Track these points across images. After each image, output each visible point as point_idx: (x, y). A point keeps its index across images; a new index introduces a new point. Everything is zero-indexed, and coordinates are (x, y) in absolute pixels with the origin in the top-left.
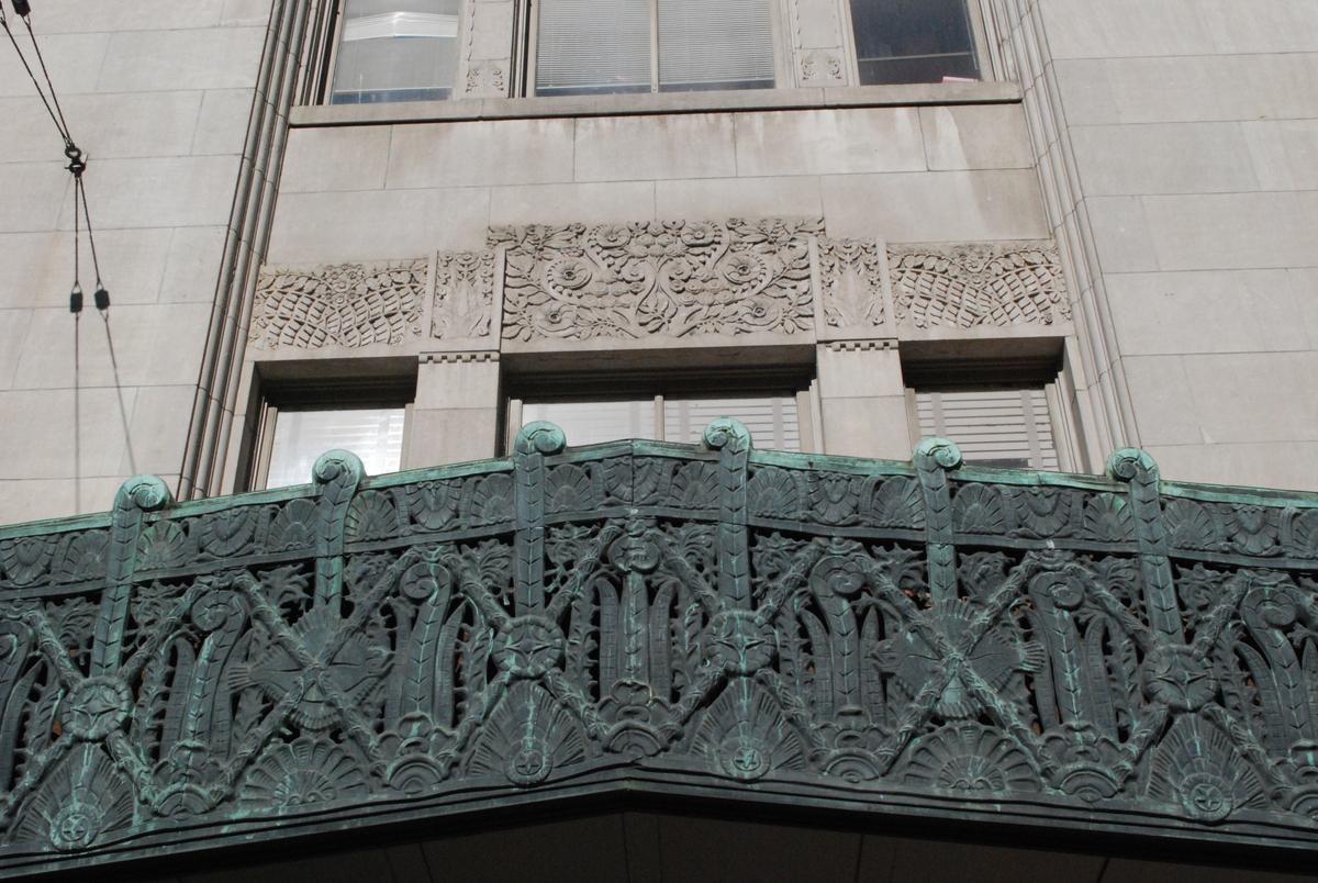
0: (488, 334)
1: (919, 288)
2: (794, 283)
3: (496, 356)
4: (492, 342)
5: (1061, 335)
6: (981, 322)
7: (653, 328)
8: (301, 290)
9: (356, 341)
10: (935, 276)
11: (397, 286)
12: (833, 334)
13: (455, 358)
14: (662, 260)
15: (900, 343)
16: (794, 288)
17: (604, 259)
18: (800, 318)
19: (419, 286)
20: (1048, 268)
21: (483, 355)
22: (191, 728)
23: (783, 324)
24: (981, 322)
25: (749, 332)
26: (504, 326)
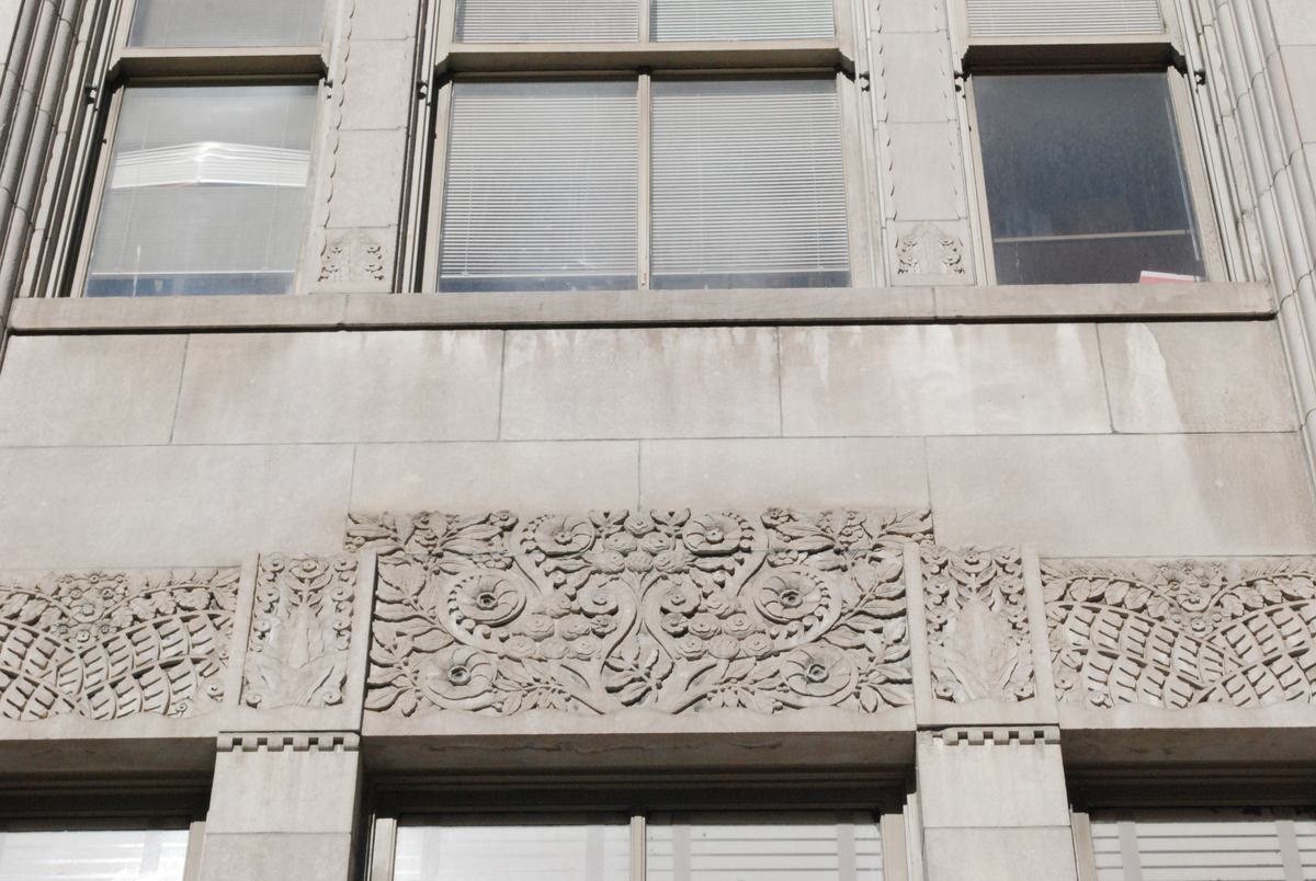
2: (879, 623)
6: (1205, 699)
10: (1124, 616)
12: (945, 714)
23: (857, 696)
24: (1205, 699)
26: (368, 687)
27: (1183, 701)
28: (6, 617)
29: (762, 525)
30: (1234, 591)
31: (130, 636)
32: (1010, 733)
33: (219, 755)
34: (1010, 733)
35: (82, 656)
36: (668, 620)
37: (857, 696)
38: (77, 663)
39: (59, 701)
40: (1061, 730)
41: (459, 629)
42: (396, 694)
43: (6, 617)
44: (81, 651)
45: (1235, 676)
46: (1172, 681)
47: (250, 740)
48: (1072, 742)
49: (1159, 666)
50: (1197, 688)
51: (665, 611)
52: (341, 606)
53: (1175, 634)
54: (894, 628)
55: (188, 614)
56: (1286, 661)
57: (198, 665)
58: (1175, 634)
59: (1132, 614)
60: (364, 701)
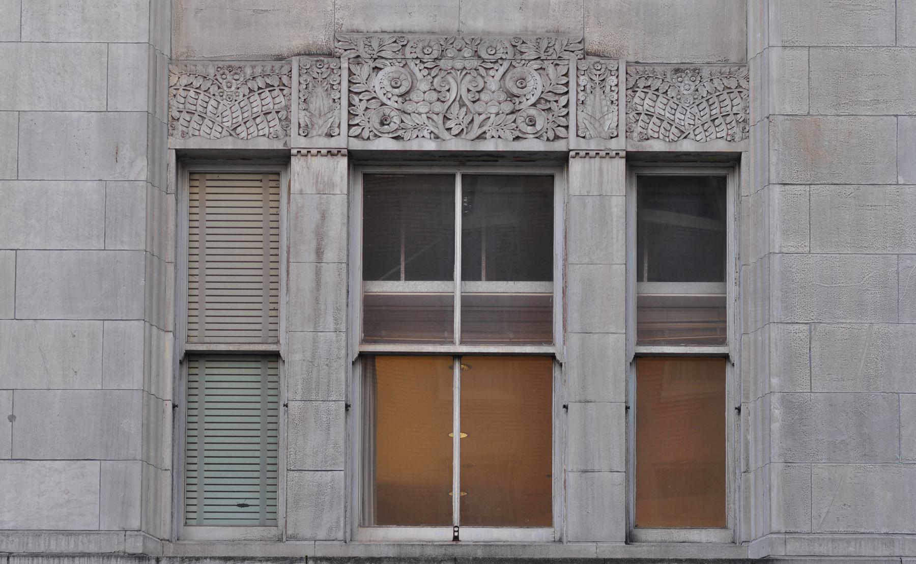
0: (617, 136)
1: (646, 107)
2: (557, 98)
3: (623, 154)
4: (340, 142)
5: (739, 150)
6: (685, 138)
7: (457, 132)
8: (657, 90)
9: (713, 136)
10: (658, 96)
11: (729, 91)
12: (583, 145)
13: (336, 153)
14: (464, 72)
15: (627, 153)
16: (556, 101)
17: (420, 70)
18: (559, 128)
19: (745, 92)
20: (282, 90)
21: (614, 153)
22: (327, 498)
23: (546, 133)
24: (685, 138)
25: (526, 138)
26: (350, 126)
27: (676, 139)
28: (654, 91)
29: (511, 46)
30: (170, 85)
31: (707, 100)
32: (576, 153)
33: (292, 157)
34: (576, 153)
35: (231, 108)
36: (470, 96)
37: (546, 133)
38: (228, 112)
39: (224, 130)
40: (348, 150)
41: (391, 102)
42: (361, 129)
43: (654, 91)
44: (230, 107)
45: (240, 125)
46: (674, 130)
47: (592, 153)
48: (633, 160)
49: (210, 119)
50: (683, 132)
51: (469, 90)
52: (334, 87)
53: (678, 105)
54: (563, 100)
55: (729, 91)
56: (274, 114)
57: (481, 116)
58: (678, 105)
59: (661, 96)
60: (348, 132)
